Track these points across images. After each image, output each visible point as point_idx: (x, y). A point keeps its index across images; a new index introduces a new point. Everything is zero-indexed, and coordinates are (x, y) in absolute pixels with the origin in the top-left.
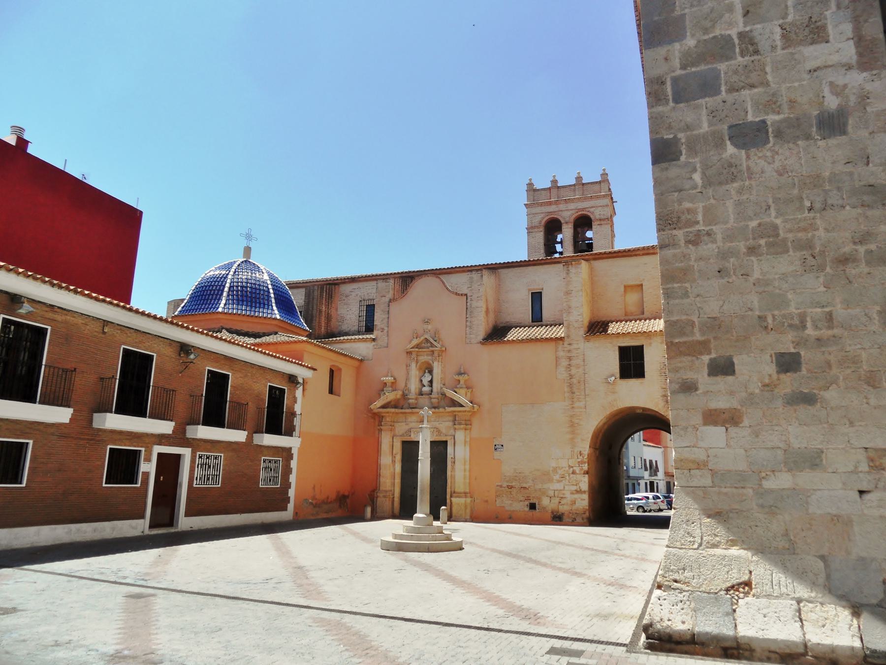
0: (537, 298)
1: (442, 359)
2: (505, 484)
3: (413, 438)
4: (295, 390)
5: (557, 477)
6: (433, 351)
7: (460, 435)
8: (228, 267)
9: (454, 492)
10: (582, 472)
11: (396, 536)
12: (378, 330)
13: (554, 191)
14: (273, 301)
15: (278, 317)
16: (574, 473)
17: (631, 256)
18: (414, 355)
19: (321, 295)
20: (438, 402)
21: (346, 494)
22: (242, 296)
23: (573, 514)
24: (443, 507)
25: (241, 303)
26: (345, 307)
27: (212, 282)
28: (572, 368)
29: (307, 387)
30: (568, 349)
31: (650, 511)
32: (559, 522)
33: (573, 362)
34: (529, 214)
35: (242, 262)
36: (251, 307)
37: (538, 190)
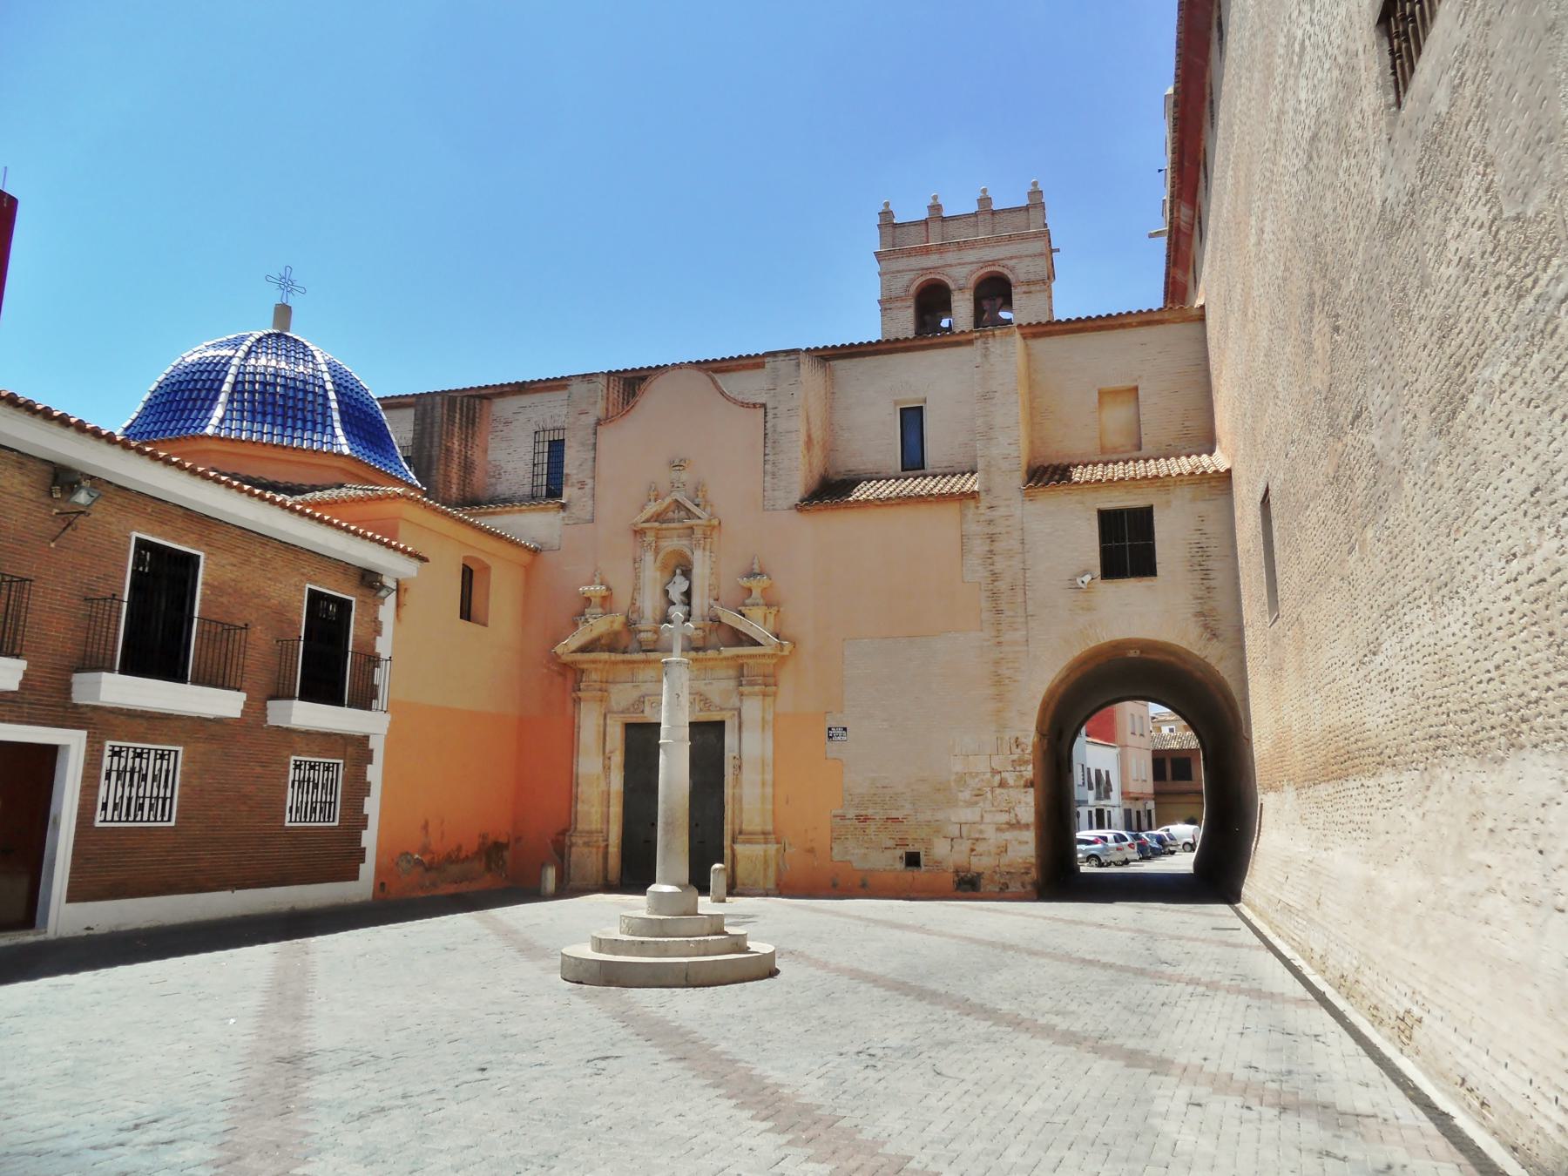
0: (912, 419)
1: (711, 543)
2: (851, 813)
3: (649, 716)
4: (376, 606)
5: (966, 795)
6: (691, 528)
7: (753, 709)
8: (236, 344)
9: (741, 833)
10: (1022, 783)
11: (600, 945)
12: (572, 485)
13: (935, 227)
14: (336, 416)
15: (346, 450)
16: (1002, 784)
17: (1113, 328)
18: (650, 538)
19: (451, 420)
20: (704, 637)
21: (503, 840)
22: (263, 403)
23: (1002, 875)
24: (717, 866)
25: (259, 418)
26: (504, 445)
27: (195, 373)
28: (995, 558)
29: (407, 599)
30: (988, 518)
31: (1109, 865)
32: (970, 893)
33: (1000, 546)
34: (885, 274)
35: (269, 335)
36: (284, 426)
37: (902, 225)
